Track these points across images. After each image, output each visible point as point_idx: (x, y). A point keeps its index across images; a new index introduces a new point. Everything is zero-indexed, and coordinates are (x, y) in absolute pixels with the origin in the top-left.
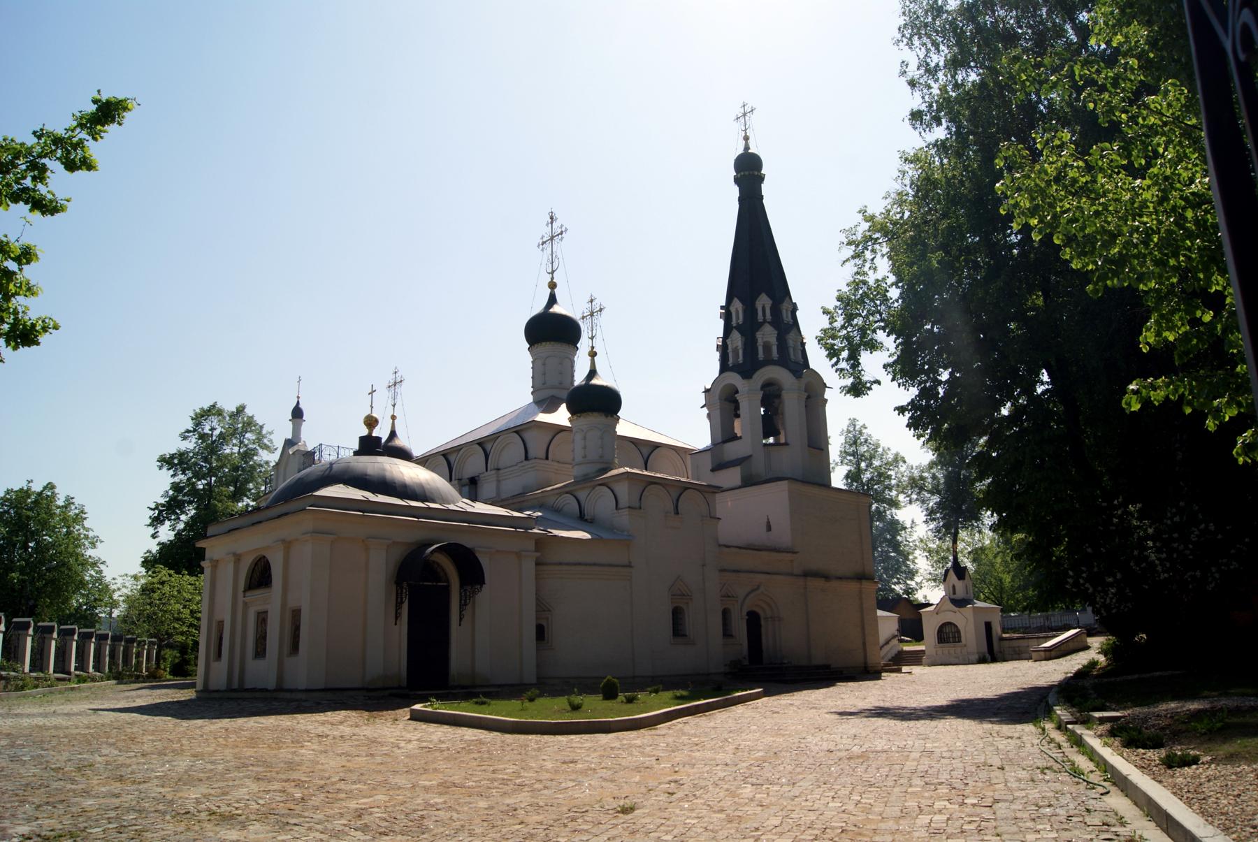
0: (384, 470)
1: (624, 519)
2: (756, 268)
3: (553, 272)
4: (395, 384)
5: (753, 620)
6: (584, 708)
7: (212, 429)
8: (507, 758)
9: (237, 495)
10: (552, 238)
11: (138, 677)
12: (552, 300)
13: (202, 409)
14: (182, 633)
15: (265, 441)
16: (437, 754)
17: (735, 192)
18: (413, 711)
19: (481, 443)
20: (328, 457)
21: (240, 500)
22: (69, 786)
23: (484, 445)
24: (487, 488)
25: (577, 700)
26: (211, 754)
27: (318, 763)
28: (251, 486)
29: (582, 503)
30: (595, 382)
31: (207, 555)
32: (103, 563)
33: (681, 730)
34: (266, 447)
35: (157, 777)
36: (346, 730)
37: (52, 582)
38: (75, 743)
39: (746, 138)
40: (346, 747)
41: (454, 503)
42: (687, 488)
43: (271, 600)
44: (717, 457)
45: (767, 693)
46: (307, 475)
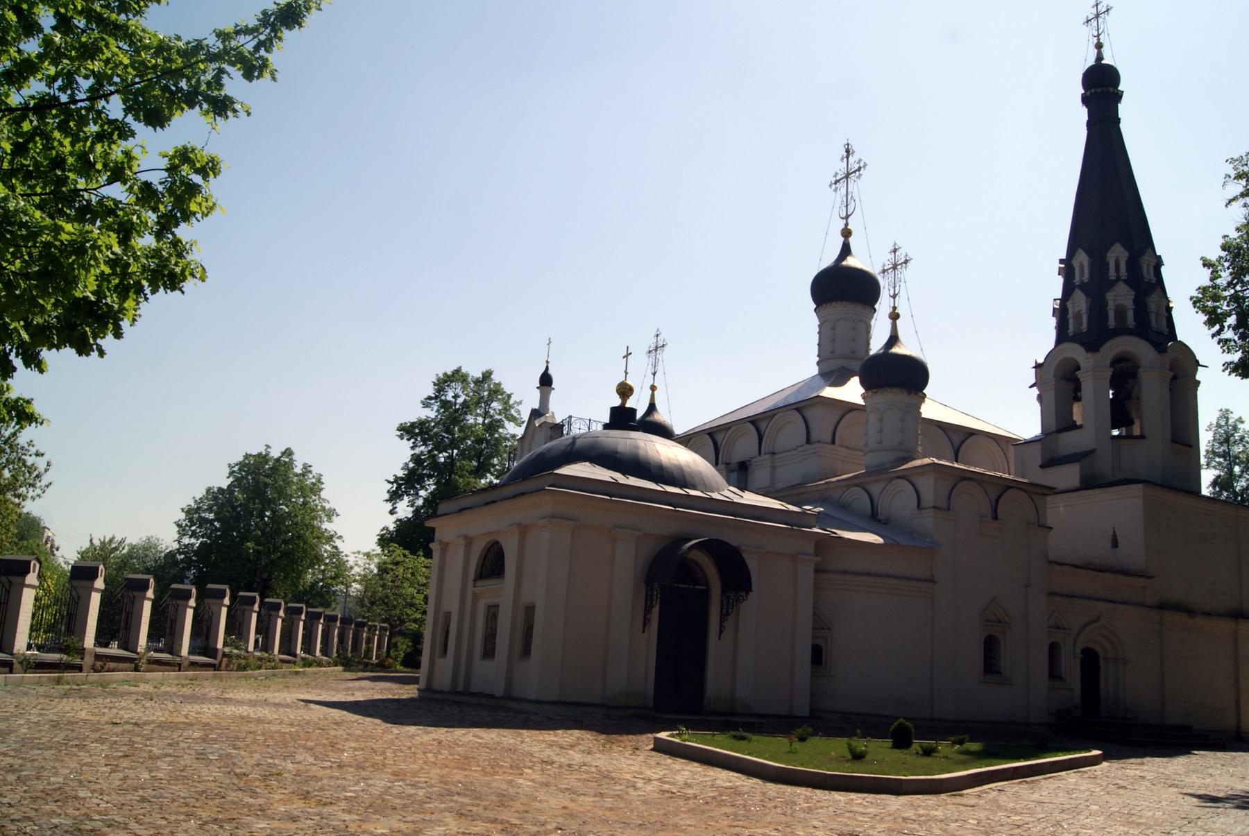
0: (637, 447)
1: (927, 521)
2: (1108, 208)
3: (847, 217)
4: (656, 349)
5: (1090, 660)
6: (869, 757)
7: (456, 396)
8: (769, 818)
9: (480, 471)
10: (847, 176)
11: (366, 665)
12: (846, 251)
13: (445, 374)
14: (415, 621)
15: (513, 411)
16: (681, 803)
17: (1083, 114)
18: (656, 739)
19: (754, 421)
20: (578, 429)
21: (483, 476)
22: (248, 800)
23: (758, 423)
24: (760, 475)
25: (861, 744)
26: (415, 774)
27: (535, 799)
28: (495, 461)
29: (876, 500)
30: (896, 350)
31: (437, 536)
32: (340, 537)
33: (995, 800)
34: (512, 419)
35: (346, 798)
36: (576, 757)
37: (286, 555)
38: (271, 742)
39: (1099, 46)
40: (571, 781)
41: (718, 491)
42: (1009, 488)
43: (503, 592)
44: (1049, 448)
45: (1106, 757)
46: (549, 450)
